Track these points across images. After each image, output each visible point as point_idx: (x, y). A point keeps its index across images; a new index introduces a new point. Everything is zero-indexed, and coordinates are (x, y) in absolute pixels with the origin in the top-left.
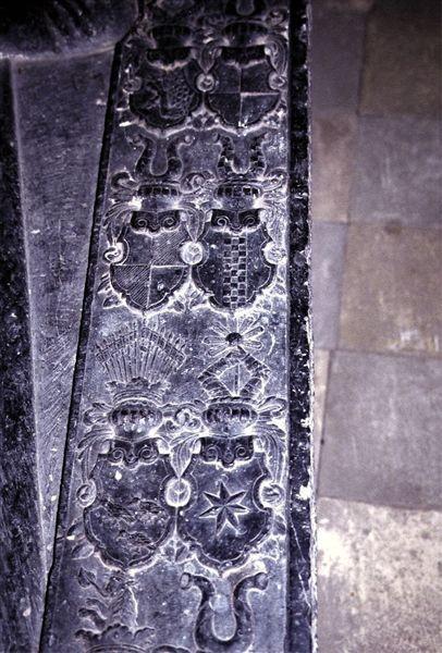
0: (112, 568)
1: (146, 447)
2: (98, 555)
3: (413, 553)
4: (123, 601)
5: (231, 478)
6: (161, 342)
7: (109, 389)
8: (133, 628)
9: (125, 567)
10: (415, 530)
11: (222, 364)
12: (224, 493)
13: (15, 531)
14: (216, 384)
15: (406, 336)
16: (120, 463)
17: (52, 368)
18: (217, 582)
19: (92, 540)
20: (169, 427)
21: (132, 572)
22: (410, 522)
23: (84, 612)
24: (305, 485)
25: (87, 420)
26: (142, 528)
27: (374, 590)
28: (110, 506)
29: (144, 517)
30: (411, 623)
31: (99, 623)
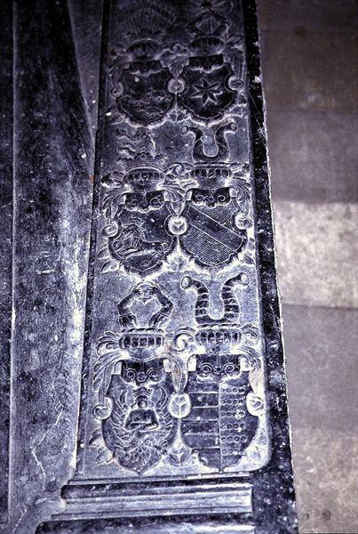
0: (137, 126)
1: (156, 65)
2: (127, 121)
3: (322, 229)
4: (147, 142)
5: (210, 76)
6: (158, 10)
7: (126, 37)
8: (153, 154)
9: (146, 124)
10: (322, 215)
11: (200, 19)
12: (206, 84)
13: (71, 116)
14: (196, 30)
15: (312, 99)
16: (138, 73)
17: (86, 34)
18: (205, 130)
19: (123, 112)
20: (168, 53)
21: (150, 127)
22: (319, 210)
23: (121, 149)
24: (258, 76)
25: (114, 53)
26: (155, 105)
27: (295, 252)
28: (133, 95)
29: (156, 99)
30: (322, 269)
31: (131, 153)
